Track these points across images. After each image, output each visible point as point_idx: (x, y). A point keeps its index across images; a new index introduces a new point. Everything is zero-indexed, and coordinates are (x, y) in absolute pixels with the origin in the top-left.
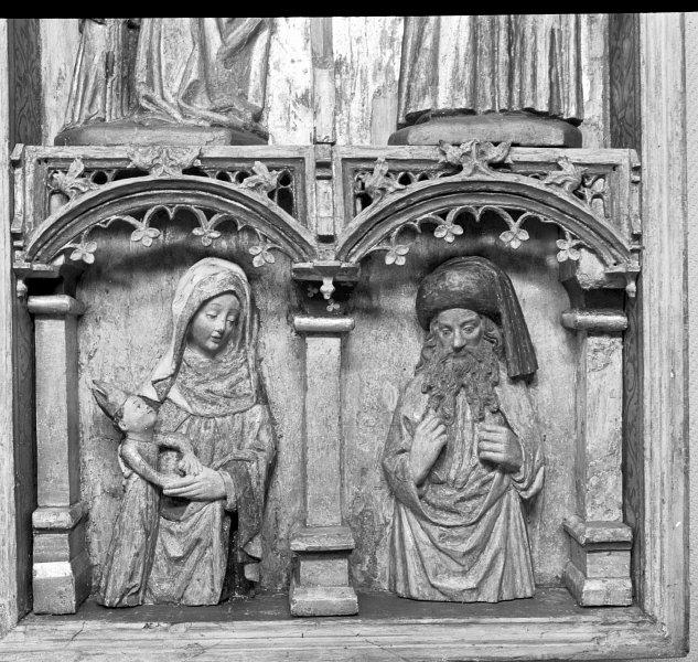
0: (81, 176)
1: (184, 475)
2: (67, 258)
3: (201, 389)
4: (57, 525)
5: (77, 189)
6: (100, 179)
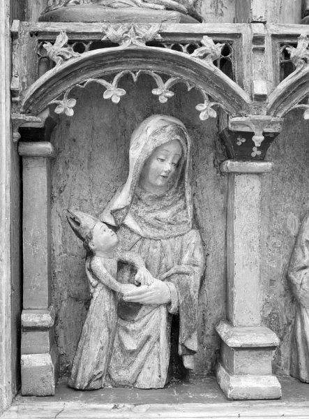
0: (65, 46)
1: (139, 284)
2: (52, 112)
3: (150, 217)
4: (40, 324)
5: (62, 56)
6: (79, 48)
